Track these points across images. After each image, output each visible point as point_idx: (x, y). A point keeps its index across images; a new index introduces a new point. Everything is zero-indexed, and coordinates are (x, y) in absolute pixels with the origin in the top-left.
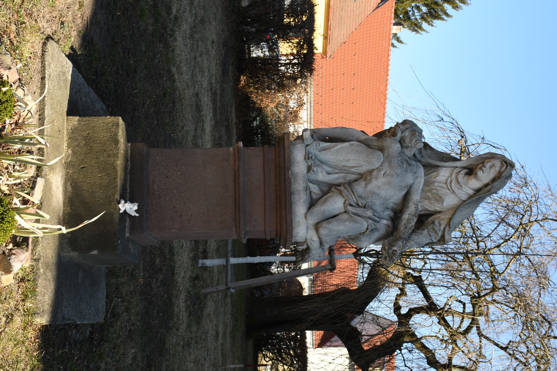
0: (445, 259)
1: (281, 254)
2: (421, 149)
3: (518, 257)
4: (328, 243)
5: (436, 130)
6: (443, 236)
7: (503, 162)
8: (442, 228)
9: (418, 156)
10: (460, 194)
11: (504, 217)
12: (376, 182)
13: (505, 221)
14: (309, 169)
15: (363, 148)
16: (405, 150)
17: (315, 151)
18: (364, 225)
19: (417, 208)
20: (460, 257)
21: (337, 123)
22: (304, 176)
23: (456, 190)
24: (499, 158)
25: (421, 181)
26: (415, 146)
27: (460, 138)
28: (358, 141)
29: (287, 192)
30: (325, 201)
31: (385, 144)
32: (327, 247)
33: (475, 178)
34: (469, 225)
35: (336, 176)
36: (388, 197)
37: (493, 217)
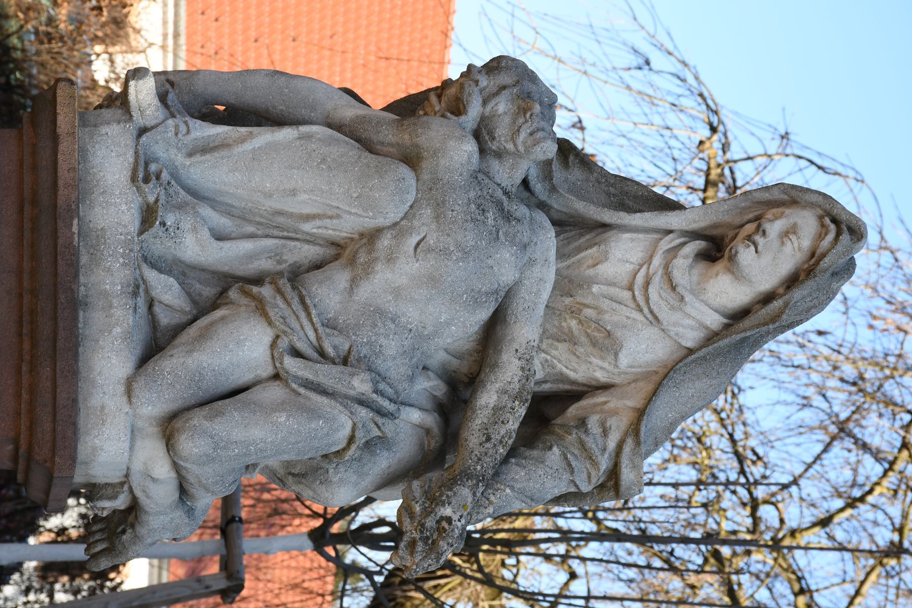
0: (642, 561)
1: (46, 537)
2: (548, 163)
3: (893, 562)
4: (207, 490)
5: (624, 100)
6: (614, 473)
7: (827, 220)
8: (612, 444)
9: (538, 187)
10: (675, 324)
11: (848, 419)
12: (389, 275)
13: (851, 435)
14: (148, 216)
15: (346, 148)
16: (495, 165)
17: (173, 151)
18: (341, 424)
19: (527, 372)
20: (690, 555)
21: (277, 57)
22: (128, 243)
23: (664, 314)
24: (812, 205)
25: (546, 274)
26: (527, 151)
27: (707, 132)
28: (330, 126)
29: (62, 297)
30: (203, 336)
31: (422, 140)
32: (208, 504)
33: (730, 271)
34: (725, 444)
35: (247, 246)
36: (430, 329)
37: (808, 416)
